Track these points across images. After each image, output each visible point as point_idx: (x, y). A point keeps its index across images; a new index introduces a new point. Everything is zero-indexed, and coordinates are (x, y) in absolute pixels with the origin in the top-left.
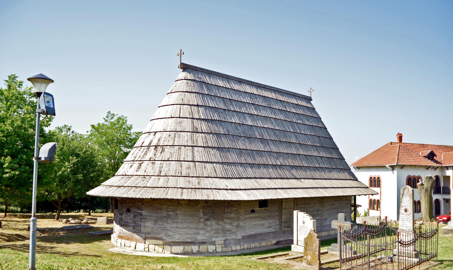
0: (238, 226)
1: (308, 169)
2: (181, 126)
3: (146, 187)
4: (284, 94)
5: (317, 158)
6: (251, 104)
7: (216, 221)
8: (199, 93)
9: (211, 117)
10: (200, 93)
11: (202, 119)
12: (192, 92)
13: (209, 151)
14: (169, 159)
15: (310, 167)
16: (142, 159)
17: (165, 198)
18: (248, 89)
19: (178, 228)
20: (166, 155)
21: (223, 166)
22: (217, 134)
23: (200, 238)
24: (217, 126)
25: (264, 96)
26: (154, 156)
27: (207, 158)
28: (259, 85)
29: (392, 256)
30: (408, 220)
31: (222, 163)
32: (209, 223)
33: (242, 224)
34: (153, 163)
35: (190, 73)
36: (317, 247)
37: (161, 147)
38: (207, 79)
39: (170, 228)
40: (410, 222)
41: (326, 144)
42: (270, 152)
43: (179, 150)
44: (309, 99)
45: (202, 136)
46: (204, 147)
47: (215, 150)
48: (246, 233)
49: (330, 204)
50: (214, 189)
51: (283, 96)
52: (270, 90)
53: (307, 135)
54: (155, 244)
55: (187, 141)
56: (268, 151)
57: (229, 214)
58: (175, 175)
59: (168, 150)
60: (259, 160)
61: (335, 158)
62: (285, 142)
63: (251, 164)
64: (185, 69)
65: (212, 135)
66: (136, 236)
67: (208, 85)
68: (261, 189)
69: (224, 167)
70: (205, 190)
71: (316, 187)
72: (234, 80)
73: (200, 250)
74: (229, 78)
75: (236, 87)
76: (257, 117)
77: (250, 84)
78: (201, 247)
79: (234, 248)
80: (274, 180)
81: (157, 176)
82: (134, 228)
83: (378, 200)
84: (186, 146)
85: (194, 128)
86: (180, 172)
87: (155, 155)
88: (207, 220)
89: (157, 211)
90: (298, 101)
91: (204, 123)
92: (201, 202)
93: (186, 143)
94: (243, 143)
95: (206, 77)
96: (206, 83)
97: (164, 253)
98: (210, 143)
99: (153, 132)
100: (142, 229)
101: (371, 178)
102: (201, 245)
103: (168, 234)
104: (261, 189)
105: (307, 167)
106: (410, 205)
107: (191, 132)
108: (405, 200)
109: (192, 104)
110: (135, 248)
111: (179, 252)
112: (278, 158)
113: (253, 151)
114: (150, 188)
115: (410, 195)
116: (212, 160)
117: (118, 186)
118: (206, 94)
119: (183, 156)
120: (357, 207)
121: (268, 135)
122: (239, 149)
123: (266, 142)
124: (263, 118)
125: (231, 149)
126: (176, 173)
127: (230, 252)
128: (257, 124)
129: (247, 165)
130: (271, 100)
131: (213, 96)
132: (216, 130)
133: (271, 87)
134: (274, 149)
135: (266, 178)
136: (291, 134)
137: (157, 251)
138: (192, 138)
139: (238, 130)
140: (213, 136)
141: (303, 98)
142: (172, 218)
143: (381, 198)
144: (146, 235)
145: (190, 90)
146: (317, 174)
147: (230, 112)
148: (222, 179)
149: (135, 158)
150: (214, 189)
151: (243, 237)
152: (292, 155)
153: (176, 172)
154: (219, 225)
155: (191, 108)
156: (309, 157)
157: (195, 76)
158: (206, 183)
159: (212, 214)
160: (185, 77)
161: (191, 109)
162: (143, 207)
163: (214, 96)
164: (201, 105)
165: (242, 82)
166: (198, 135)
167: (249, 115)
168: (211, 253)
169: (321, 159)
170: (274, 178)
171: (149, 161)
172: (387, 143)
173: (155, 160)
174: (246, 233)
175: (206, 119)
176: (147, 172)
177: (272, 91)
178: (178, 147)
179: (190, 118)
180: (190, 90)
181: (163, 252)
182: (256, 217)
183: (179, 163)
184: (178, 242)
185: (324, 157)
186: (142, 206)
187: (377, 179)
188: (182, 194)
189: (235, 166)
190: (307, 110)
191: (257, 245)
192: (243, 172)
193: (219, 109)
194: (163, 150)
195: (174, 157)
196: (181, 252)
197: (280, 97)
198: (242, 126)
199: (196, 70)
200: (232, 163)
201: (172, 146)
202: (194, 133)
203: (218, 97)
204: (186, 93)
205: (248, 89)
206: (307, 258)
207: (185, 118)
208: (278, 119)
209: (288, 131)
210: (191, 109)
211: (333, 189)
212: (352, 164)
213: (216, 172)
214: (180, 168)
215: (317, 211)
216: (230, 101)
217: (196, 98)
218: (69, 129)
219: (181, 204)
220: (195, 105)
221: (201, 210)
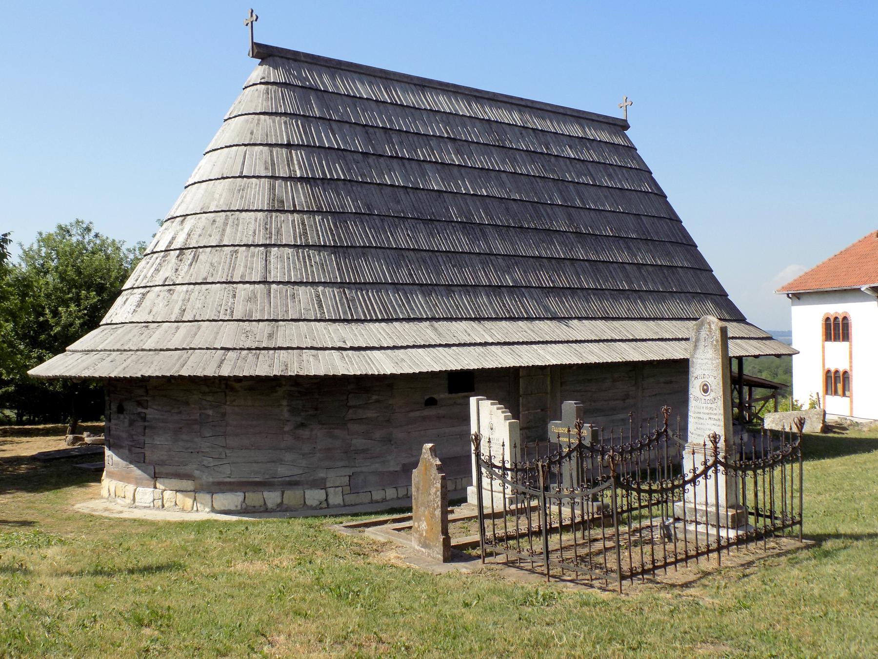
0: (388, 440)
1: (594, 294)
2: (242, 197)
3: (143, 350)
4: (546, 114)
5: (627, 267)
6: (446, 140)
8: (296, 115)
9: (324, 173)
10: (299, 115)
11: (297, 178)
12: (276, 114)
13: (309, 256)
14: (206, 279)
15: (603, 290)
17: (176, 374)
18: (444, 103)
19: (229, 448)
20: (201, 271)
21: (344, 290)
22: (336, 215)
23: (283, 471)
24: (338, 196)
25: (489, 121)
26: (174, 275)
27: (301, 274)
28: (477, 94)
29: (671, 520)
30: (712, 416)
31: (342, 285)
32: (305, 433)
33: (398, 434)
34: (170, 290)
35: (275, 67)
36: (437, 497)
38: (326, 82)
40: (718, 423)
42: (489, 254)
43: (232, 255)
44: (622, 126)
45: (293, 221)
46: (295, 246)
47: (324, 254)
48: (413, 456)
49: (662, 380)
50: (307, 348)
51: (544, 119)
52: (508, 105)
53: (603, 212)
54: (177, 488)
55: (255, 233)
56: (480, 254)
57: (360, 411)
58: (216, 318)
60: (451, 275)
61: (681, 267)
62: (536, 229)
63: (427, 285)
64: (266, 58)
65: (320, 217)
66: (136, 472)
67: (325, 95)
68: (440, 345)
69: (345, 294)
70: (282, 351)
71: (610, 338)
72: (403, 82)
73: (284, 503)
74: (392, 77)
75: (409, 99)
76: (459, 171)
77: (451, 91)
78: (287, 493)
79: (377, 495)
80: (488, 324)
81: (175, 322)
82: (130, 450)
83: (845, 372)
84: (252, 245)
85: (273, 200)
86: (229, 311)
87: (177, 270)
88: (302, 425)
89: (179, 408)
90: (587, 130)
91: (303, 188)
92: (284, 383)
93: (251, 238)
94: (408, 235)
95: (354, 83)
96: (321, 91)
97: (197, 510)
98: (312, 237)
99: (181, 216)
100: (148, 453)
101: (828, 319)
103: (205, 463)
104: (440, 345)
105: (593, 289)
106: (715, 374)
107: (267, 210)
108: (703, 357)
109: (274, 142)
110: (134, 500)
111: (233, 508)
112: (508, 270)
113: (437, 254)
114: (151, 353)
115: (715, 343)
116: (313, 276)
117: (85, 351)
118: (316, 118)
119: (242, 269)
121: (486, 213)
122: (396, 248)
124: (476, 172)
125: (373, 250)
126: (219, 312)
127: (365, 504)
128: (459, 187)
129: (415, 287)
130: (507, 129)
131: (335, 121)
132: (333, 204)
133: (512, 97)
134: (500, 247)
135: (466, 319)
136: (557, 209)
137: (181, 507)
138: (268, 227)
139: (398, 202)
140: (323, 220)
141: (605, 123)
142: (212, 424)
143: (851, 367)
144: (156, 468)
145: (272, 108)
146: (622, 308)
147: (382, 160)
148: (337, 324)
149: (136, 280)
150: (307, 348)
152: (553, 261)
153: (219, 309)
155: (271, 152)
156: (601, 266)
157: (290, 73)
158: (288, 334)
159: (312, 412)
161: (272, 156)
162: (149, 399)
163: (338, 121)
164: (298, 145)
165: (428, 87)
166: (282, 217)
167: (437, 165)
168: (315, 508)
169: (639, 269)
170: (489, 319)
172: (867, 234)
175: (308, 178)
176: (153, 313)
177: (514, 107)
179: (266, 177)
180: (272, 108)
181: (195, 509)
182: (439, 418)
183: (230, 287)
184: (230, 483)
185: (647, 265)
186: (145, 398)
187: (841, 320)
188: (221, 363)
189: (377, 292)
190: (610, 151)
192: (399, 306)
193: (349, 153)
194: (195, 258)
196: (237, 507)
197: (534, 122)
198: (413, 193)
199: (295, 60)
200: (369, 283)
201: (218, 248)
202: (274, 214)
203: (350, 123)
204: (262, 117)
205: (444, 103)
206: (419, 526)
207: (254, 177)
208: (521, 174)
209: (548, 204)
210: (272, 156)
211: (660, 343)
212: (783, 288)
213: (320, 306)
214: (231, 300)
215: (624, 400)
216: (385, 133)
217: (286, 128)
218: (88, 230)
219: (233, 389)
220: (281, 146)
221: (285, 403)
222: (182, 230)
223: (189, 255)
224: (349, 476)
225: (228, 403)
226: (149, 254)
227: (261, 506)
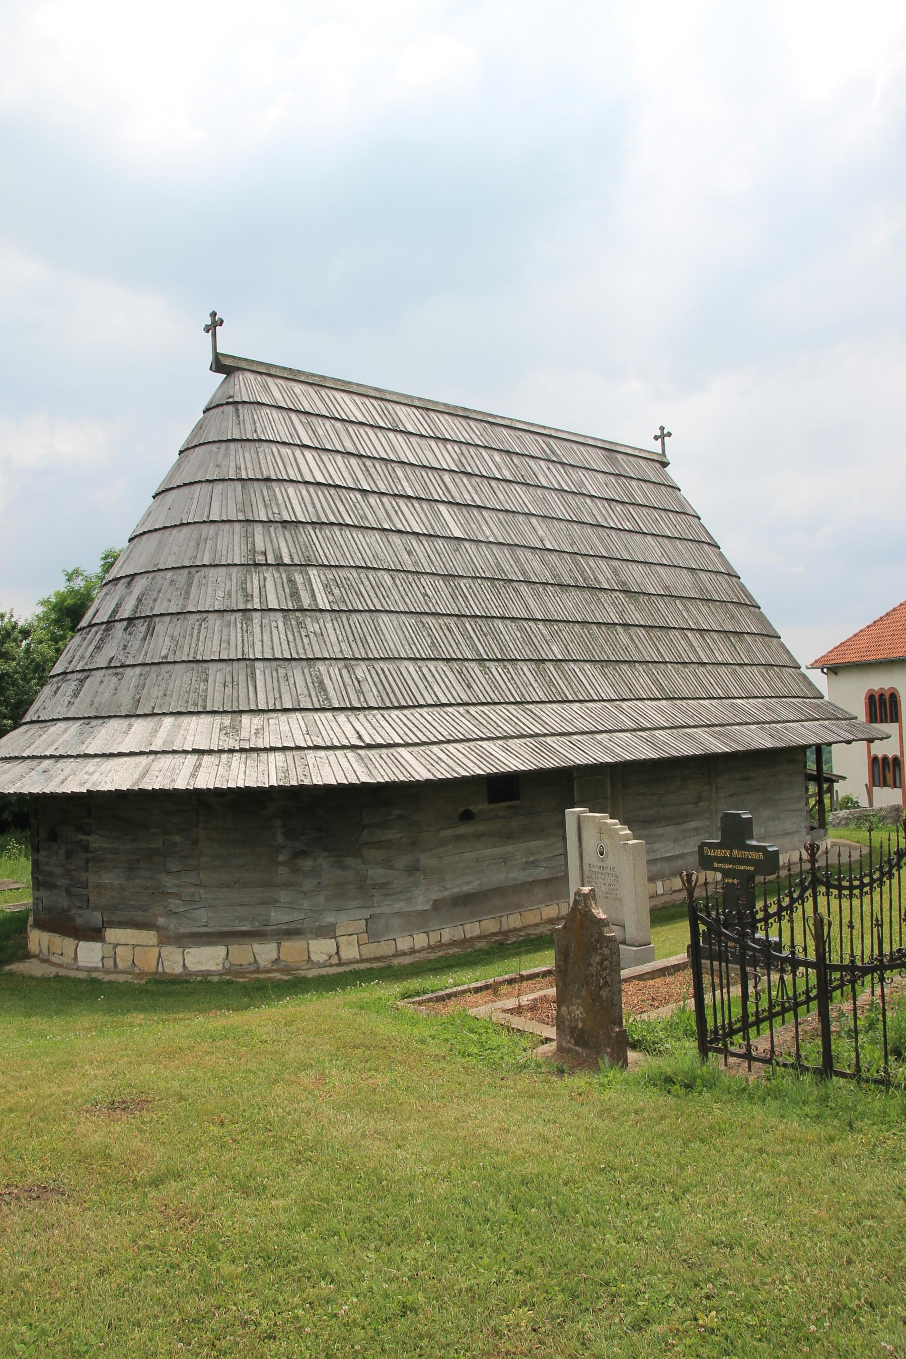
0: (413, 869)
7: (333, 857)
14: (166, 657)
16: (86, 664)
17: (136, 788)
26: (122, 653)
28: (491, 420)
32: (307, 864)
33: (426, 860)
37: (145, 622)
39: (175, 890)
41: (717, 591)
43: (200, 625)
48: (446, 889)
58: (183, 710)
59: (164, 628)
73: (282, 958)
78: (286, 944)
87: (125, 647)
99: (127, 576)
100: (93, 899)
102: (286, 940)
120: (835, 781)
123: (510, 590)
143: (902, 752)
149: (70, 662)
151: (437, 905)
154: (345, 868)
160: (231, 397)
171: (106, 668)
173: (122, 666)
174: (446, 889)
176: (96, 705)
178: (198, 616)
182: (478, 836)
184: (207, 935)
186: (88, 821)
191: (490, 926)
194: (150, 631)
195: (186, 649)
215: (696, 803)
221: (278, 823)
222: (130, 594)
223: (141, 628)
224: (366, 919)
225: (201, 825)
226: (85, 628)
227: (250, 964)
